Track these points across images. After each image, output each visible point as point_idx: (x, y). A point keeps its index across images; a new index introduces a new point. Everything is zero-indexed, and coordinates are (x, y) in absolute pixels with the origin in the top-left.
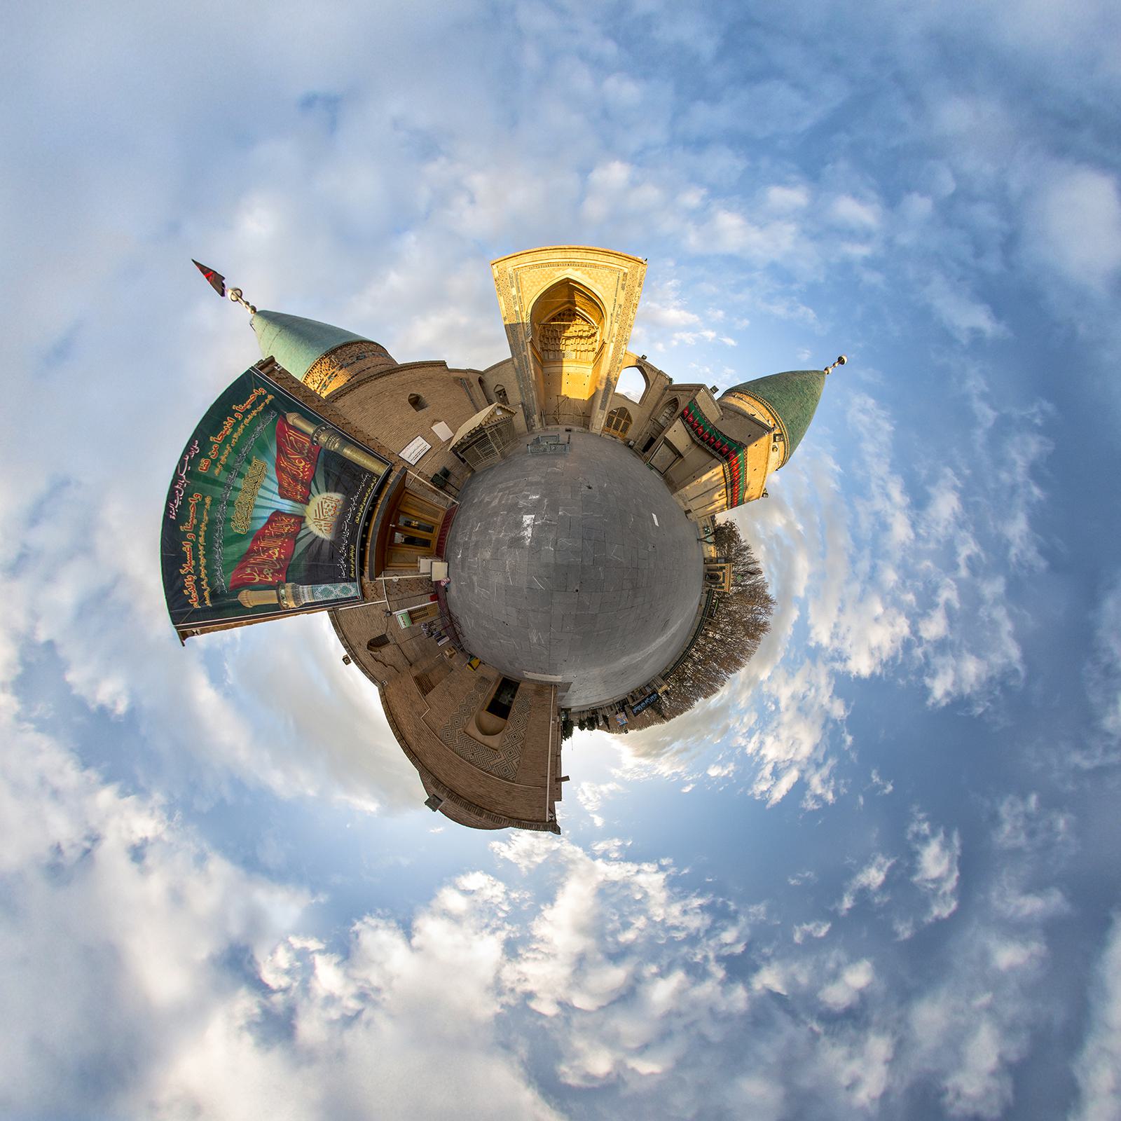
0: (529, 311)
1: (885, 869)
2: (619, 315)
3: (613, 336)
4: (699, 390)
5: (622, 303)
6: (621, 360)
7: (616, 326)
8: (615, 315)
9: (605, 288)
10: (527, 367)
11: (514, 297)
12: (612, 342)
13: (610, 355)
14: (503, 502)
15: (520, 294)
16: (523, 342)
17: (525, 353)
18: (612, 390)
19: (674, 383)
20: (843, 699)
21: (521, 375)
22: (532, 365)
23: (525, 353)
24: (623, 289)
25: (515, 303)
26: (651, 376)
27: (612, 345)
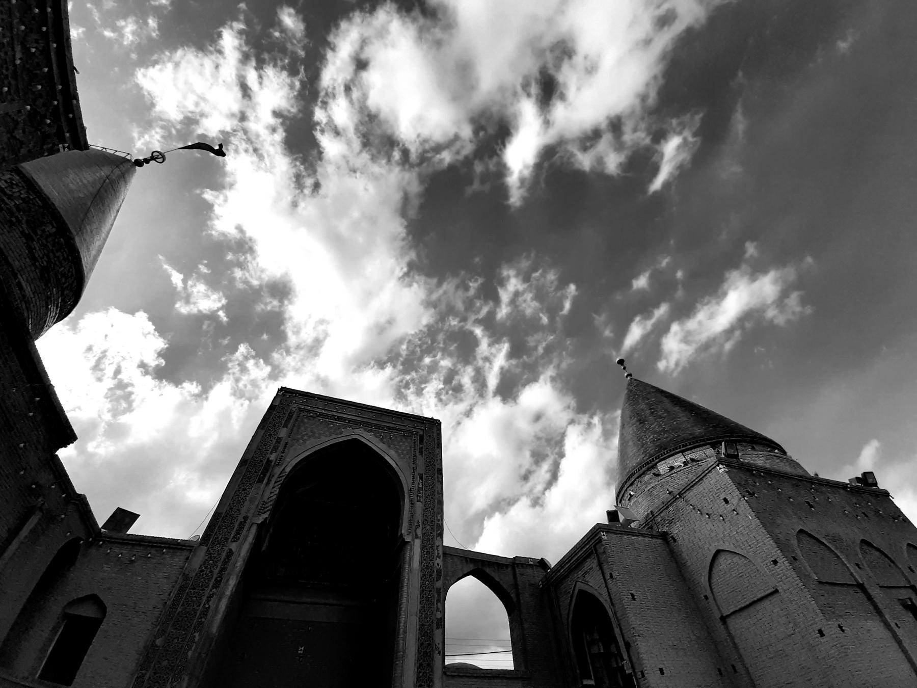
0: (288, 470)
1: (322, 94)
2: (421, 489)
3: (418, 526)
4: (600, 540)
5: (423, 472)
6: (439, 572)
7: (419, 506)
8: (416, 489)
9: (399, 455)
10: (217, 584)
11: (279, 440)
12: (417, 537)
13: (416, 564)
14: (179, 609)
15: (289, 440)
16: (246, 518)
17: (234, 546)
18: (438, 658)
19: (553, 561)
20: (279, 11)
21: (180, 612)
22: (233, 582)
23: (234, 546)
24: (421, 453)
25: (275, 449)
26: (505, 579)
27: (417, 544)
